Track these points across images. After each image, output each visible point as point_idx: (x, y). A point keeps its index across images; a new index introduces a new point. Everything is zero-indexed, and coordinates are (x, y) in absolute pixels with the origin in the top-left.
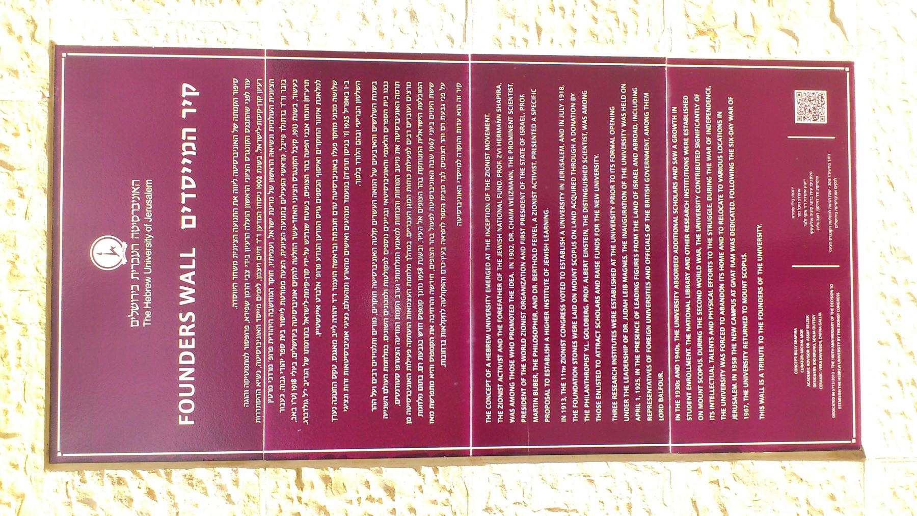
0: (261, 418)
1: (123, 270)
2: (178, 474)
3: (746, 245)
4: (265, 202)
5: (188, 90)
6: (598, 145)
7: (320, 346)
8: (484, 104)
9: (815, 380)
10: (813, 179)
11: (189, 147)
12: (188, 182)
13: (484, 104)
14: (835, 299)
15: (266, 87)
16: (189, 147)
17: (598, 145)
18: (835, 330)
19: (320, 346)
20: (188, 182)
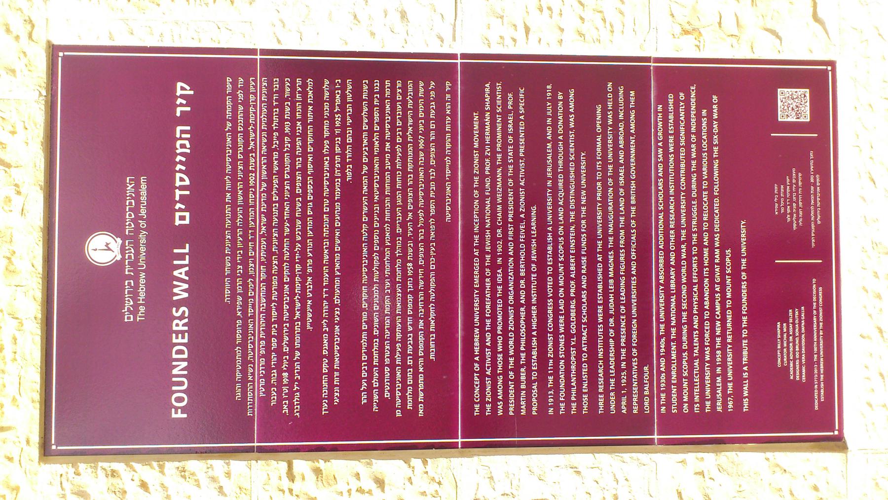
0: (253, 411)
1: (118, 266)
2: (171, 466)
3: (730, 241)
4: (257, 199)
5: (182, 89)
6: (585, 142)
7: (311, 340)
8: (473, 102)
9: (798, 373)
10: (797, 176)
11: (183, 144)
12: (181, 180)
13: (473, 102)
14: (817, 293)
15: (259, 85)
16: (183, 144)
17: (585, 142)
18: (818, 323)
19: (311, 340)
20: (181, 180)
